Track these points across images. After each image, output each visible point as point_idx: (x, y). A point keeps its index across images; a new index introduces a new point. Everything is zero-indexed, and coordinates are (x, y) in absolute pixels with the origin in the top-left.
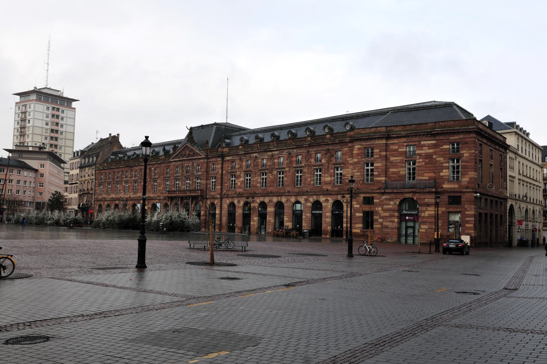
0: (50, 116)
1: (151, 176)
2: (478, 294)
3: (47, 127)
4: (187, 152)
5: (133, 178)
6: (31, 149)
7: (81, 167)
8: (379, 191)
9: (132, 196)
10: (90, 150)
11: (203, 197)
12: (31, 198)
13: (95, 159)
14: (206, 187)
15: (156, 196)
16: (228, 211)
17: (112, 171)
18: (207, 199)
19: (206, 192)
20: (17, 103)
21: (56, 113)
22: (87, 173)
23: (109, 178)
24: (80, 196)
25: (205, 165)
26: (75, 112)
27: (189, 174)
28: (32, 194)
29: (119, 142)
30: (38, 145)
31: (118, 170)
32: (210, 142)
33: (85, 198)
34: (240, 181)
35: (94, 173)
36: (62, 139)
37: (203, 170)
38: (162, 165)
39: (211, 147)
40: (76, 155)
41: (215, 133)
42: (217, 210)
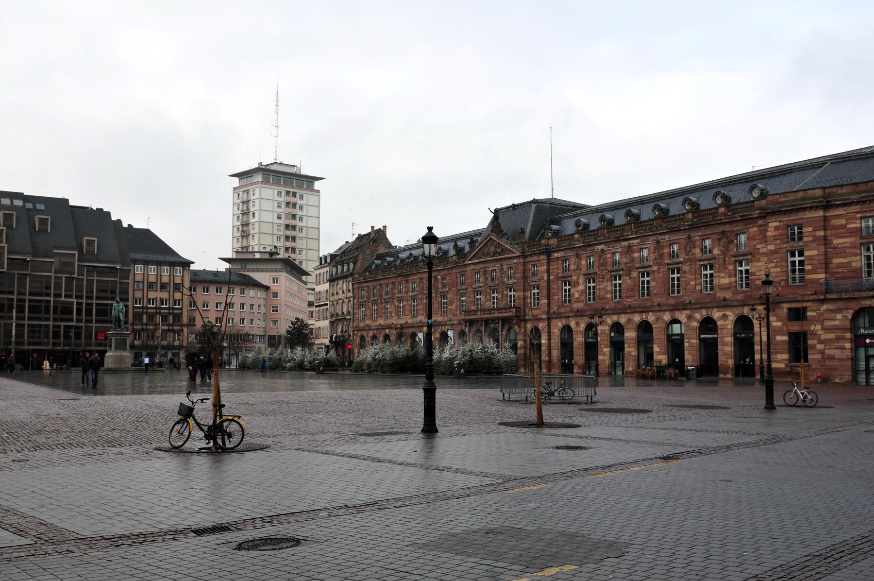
0: (283, 205)
4: (492, 249)
6: (257, 256)
7: (332, 280)
8: (815, 297)
9: (409, 321)
10: (344, 252)
11: (520, 318)
12: (262, 329)
13: (351, 266)
14: (525, 302)
20: (235, 189)
23: (374, 295)
24: (332, 323)
25: (521, 268)
27: (497, 283)
29: (387, 239)
30: (268, 250)
31: (387, 281)
32: (528, 231)
33: (340, 326)
34: (578, 291)
35: (351, 288)
36: (301, 239)
37: (518, 275)
38: (454, 271)
41: (535, 215)
42: (543, 338)
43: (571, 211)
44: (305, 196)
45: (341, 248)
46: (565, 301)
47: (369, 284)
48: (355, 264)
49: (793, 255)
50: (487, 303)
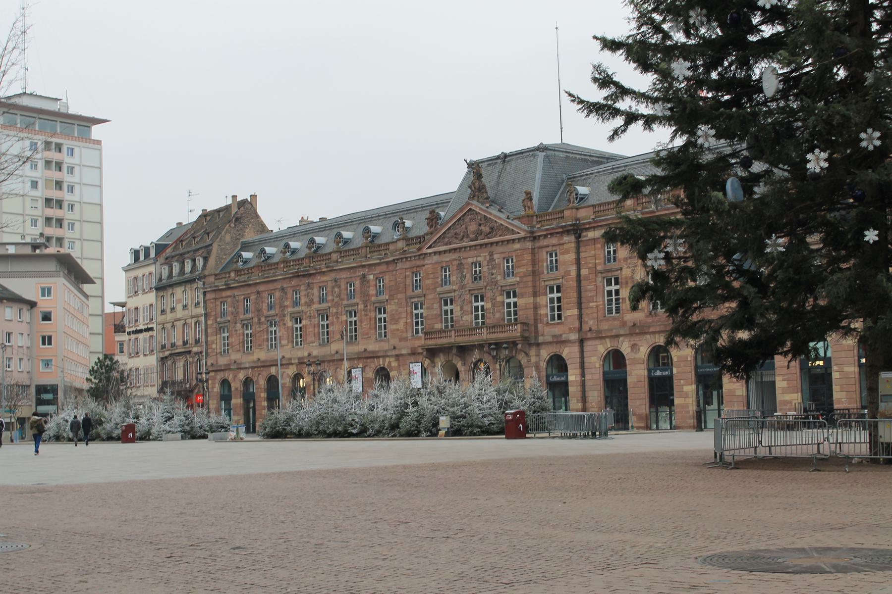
1: (368, 295)
2: (234, 549)
3: (34, 193)
4: (473, 227)
5: (316, 306)
6: (12, 250)
7: (161, 288)
9: (315, 353)
10: (180, 240)
11: (530, 341)
12: (25, 375)
13: (200, 263)
14: (536, 314)
15: (386, 346)
16: (604, 373)
17: (254, 289)
18: (538, 345)
19: (536, 327)
21: (53, 155)
22: (179, 301)
23: (246, 311)
24: (163, 360)
25: (528, 257)
26: (100, 150)
27: (482, 283)
28: (26, 366)
29: (257, 216)
30: (28, 240)
31: (270, 287)
32: (536, 197)
33: (180, 364)
35: (201, 298)
37: (522, 270)
38: (400, 265)
39: (540, 209)
40: (142, 258)
41: (544, 171)
42: (570, 372)
43: (599, 163)
44: (76, 151)
45: (171, 232)
46: (610, 311)
47: (236, 292)
48: (206, 259)
49: (446, 304)
50: (465, 318)
